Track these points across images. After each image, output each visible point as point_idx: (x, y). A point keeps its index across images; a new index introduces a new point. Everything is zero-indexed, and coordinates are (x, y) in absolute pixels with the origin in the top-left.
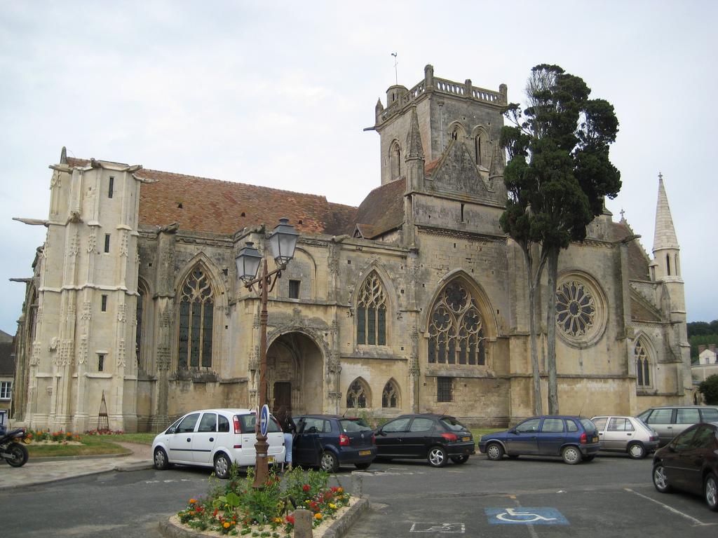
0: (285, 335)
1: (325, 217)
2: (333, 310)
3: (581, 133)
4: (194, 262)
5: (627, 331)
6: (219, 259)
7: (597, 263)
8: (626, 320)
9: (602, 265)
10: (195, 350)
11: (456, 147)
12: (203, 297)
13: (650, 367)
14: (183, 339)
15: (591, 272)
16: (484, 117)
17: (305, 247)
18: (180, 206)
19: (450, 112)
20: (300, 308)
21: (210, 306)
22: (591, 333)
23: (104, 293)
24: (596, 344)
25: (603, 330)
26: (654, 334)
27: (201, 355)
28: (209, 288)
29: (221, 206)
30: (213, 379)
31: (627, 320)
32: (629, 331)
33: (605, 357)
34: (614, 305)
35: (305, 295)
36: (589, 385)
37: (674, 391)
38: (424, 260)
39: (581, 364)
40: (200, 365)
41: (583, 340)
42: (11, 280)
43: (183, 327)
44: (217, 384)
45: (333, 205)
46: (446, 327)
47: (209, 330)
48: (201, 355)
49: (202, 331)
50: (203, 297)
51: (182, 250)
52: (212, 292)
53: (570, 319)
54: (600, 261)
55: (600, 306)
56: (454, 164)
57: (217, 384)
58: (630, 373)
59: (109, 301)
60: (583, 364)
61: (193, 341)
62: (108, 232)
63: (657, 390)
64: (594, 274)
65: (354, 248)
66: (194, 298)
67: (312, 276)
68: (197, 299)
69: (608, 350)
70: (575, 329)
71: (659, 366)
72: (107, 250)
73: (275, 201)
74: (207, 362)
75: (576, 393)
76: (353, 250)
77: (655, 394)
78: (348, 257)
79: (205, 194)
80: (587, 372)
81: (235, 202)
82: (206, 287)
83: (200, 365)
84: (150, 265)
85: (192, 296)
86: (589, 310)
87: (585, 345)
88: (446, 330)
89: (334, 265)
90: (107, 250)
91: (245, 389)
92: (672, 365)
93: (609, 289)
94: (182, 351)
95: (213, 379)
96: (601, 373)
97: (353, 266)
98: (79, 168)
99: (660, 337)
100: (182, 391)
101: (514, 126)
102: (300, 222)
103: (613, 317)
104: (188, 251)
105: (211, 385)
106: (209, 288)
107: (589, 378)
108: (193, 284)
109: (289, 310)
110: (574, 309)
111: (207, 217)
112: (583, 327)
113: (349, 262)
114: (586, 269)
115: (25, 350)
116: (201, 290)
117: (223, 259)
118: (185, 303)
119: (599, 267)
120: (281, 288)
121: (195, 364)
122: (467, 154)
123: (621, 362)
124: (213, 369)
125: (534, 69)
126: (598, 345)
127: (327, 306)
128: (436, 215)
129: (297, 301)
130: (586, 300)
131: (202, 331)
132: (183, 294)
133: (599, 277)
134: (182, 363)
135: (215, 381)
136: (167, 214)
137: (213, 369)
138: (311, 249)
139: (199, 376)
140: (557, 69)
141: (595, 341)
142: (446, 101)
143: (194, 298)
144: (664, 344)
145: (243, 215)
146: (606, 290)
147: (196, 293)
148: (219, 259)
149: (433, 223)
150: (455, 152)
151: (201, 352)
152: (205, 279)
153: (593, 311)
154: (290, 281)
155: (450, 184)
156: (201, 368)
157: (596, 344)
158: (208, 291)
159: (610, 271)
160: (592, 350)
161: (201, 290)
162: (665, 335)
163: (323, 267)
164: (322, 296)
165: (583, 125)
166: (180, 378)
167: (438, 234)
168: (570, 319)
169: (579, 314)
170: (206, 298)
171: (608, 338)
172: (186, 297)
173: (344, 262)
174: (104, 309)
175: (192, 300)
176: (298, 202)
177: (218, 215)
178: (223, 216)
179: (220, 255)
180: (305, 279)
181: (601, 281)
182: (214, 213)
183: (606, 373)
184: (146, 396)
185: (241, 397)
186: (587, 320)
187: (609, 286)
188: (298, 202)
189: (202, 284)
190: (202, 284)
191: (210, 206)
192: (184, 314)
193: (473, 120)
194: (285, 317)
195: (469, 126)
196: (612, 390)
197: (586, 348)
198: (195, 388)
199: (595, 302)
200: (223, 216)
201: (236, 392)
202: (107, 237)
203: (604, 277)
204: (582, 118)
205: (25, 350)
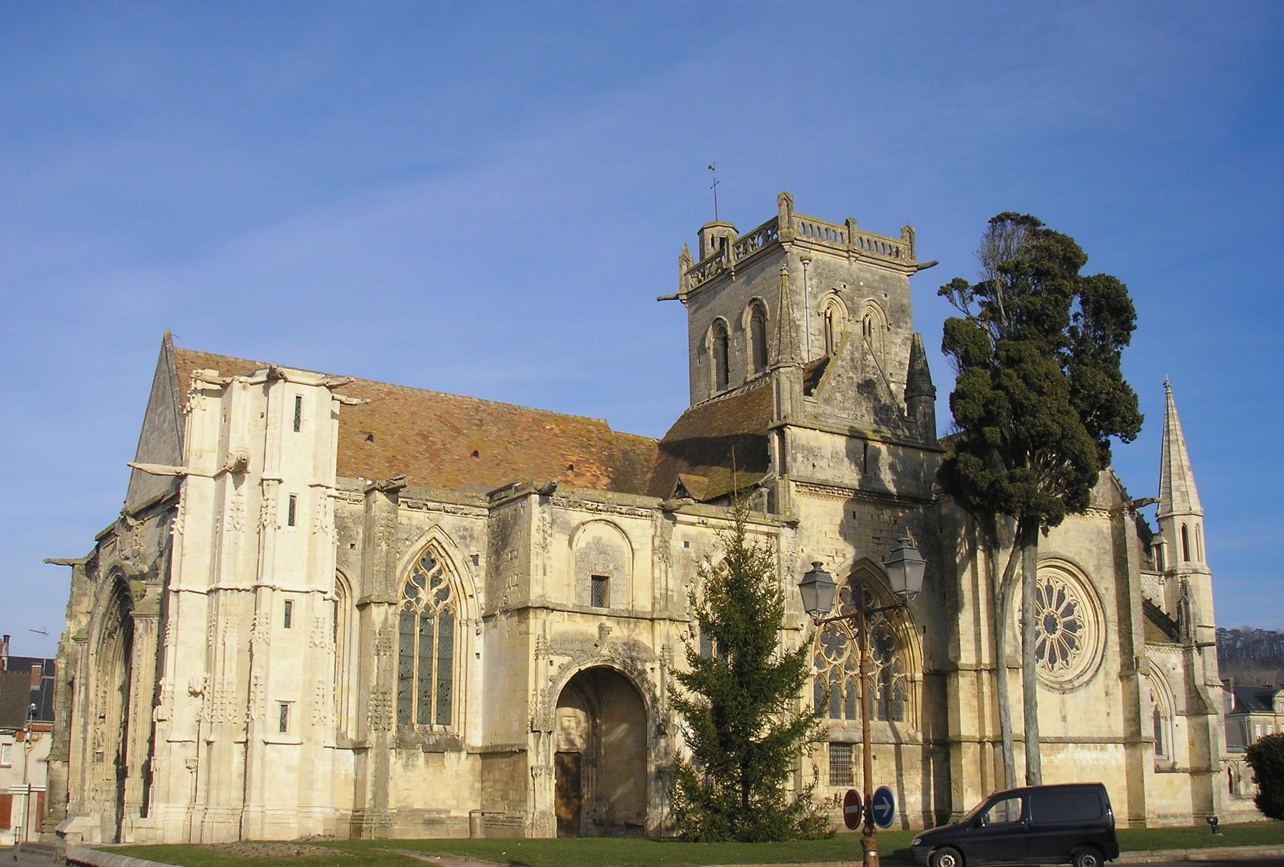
0: (587, 670)
1: (611, 457)
2: (661, 628)
3: (1073, 331)
4: (423, 541)
5: (1137, 661)
6: (464, 537)
7: (1087, 544)
8: (1135, 643)
9: (1094, 549)
10: (425, 694)
11: (852, 345)
12: (437, 603)
13: (1162, 721)
14: (404, 678)
15: (1077, 560)
16: (876, 284)
17: (615, 518)
18: (370, 438)
19: (820, 275)
20: (609, 624)
21: (447, 619)
22: (1081, 659)
23: (288, 596)
24: (1087, 683)
25: (1098, 659)
26: (1169, 666)
27: (434, 704)
28: (447, 589)
29: (437, 439)
30: (455, 745)
31: (1138, 641)
32: (1141, 661)
33: (1102, 707)
34: (1116, 617)
35: (617, 601)
36: (1077, 756)
37: (1203, 765)
38: (805, 541)
39: (1064, 719)
40: (433, 721)
41: (1067, 678)
42: (48, 562)
43: (405, 658)
44: (464, 754)
45: (618, 437)
46: (840, 654)
47: (446, 662)
48: (434, 704)
49: (435, 662)
50: (437, 603)
51: (405, 521)
52: (451, 594)
53: (1044, 641)
54: (1091, 541)
55: (1092, 619)
56: (851, 374)
57: (464, 754)
58: (1144, 734)
59: (296, 612)
60: (1068, 718)
61: (421, 680)
62: (294, 491)
63: (1174, 763)
64: (1082, 564)
65: (695, 519)
66: (423, 603)
67: (627, 570)
68: (427, 607)
69: (1107, 694)
70: (1052, 660)
71: (1178, 719)
72: (291, 523)
73: (524, 429)
74: (445, 718)
75: (1057, 768)
76: (693, 524)
77: (1173, 770)
78: (684, 536)
79: (406, 415)
80: (1073, 733)
81: (459, 431)
82: (442, 586)
83: (433, 721)
84: (352, 545)
85: (418, 600)
86: (1072, 626)
87: (1070, 686)
88: (840, 661)
89: (662, 551)
90: (291, 523)
91: (521, 764)
92: (1200, 719)
93: (1107, 589)
94: (404, 698)
95: (455, 745)
96: (1095, 734)
97: (691, 549)
98: (243, 379)
99: (1180, 670)
100: (406, 766)
101: (963, 317)
102: (571, 468)
103: (1114, 638)
104: (414, 523)
105: (451, 757)
106: (447, 589)
107: (1076, 741)
108: (421, 580)
109: (590, 627)
110: (1051, 625)
111: (416, 458)
112: (1064, 656)
113: (687, 545)
114: (1070, 555)
115: (87, 689)
116: (435, 590)
117: (472, 537)
118: (407, 616)
119: (1090, 551)
120: (579, 589)
121: (424, 719)
122: (870, 357)
123: (1129, 716)
124: (453, 729)
125: (993, 221)
126: (1091, 685)
127: (652, 620)
128: (824, 463)
129: (605, 611)
130: (1069, 610)
131: (435, 662)
132: (404, 598)
133: (1090, 569)
134: (404, 716)
135: (459, 750)
136: (349, 453)
137: (453, 729)
138: (624, 522)
139: (432, 740)
140: (1030, 222)
141: (1086, 677)
142: (813, 254)
143: (423, 603)
144: (1186, 683)
145: (476, 454)
146: (1102, 591)
147: (426, 595)
148: (464, 537)
149: (820, 476)
150: (852, 353)
151: (434, 699)
152: (440, 572)
153: (1080, 627)
154: (594, 577)
155: (844, 409)
156: (436, 728)
157: (1087, 683)
158: (444, 594)
159: (1109, 559)
160: (1082, 693)
161: (435, 590)
162: (1188, 667)
163: (644, 555)
164: (643, 603)
165: (1075, 316)
166: (402, 743)
167: (827, 496)
168: (1044, 641)
169: (1058, 633)
170: (442, 604)
171: (1106, 674)
172: (409, 602)
173: (676, 544)
174: (288, 624)
175: (420, 609)
176: (563, 431)
177: (434, 454)
178: (443, 457)
179: (465, 529)
180: (616, 574)
181: (1093, 576)
182: (426, 451)
183: (1104, 734)
184: (346, 776)
185: (512, 778)
186: (1072, 644)
187: (1107, 586)
188: (563, 431)
189: (436, 581)
190: (436, 581)
191: (419, 439)
192: (406, 635)
193: (859, 289)
194: (584, 639)
195: (852, 301)
196: (1114, 762)
197: (1072, 690)
198: (427, 762)
199: (1085, 612)
200: (443, 457)
201: (290, 768)
202: (293, 499)
203: (1098, 568)
204: (1075, 306)
205: (87, 689)
